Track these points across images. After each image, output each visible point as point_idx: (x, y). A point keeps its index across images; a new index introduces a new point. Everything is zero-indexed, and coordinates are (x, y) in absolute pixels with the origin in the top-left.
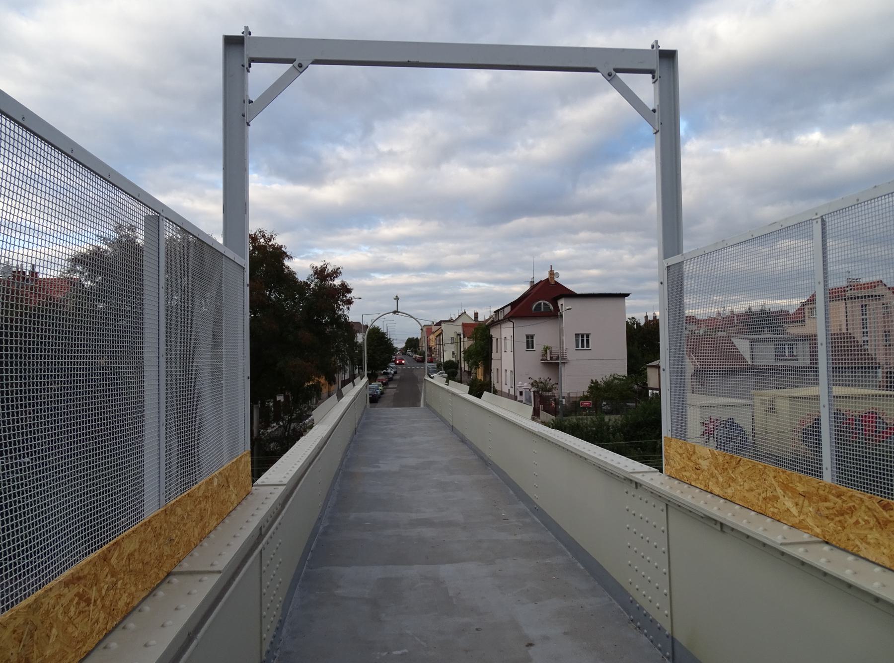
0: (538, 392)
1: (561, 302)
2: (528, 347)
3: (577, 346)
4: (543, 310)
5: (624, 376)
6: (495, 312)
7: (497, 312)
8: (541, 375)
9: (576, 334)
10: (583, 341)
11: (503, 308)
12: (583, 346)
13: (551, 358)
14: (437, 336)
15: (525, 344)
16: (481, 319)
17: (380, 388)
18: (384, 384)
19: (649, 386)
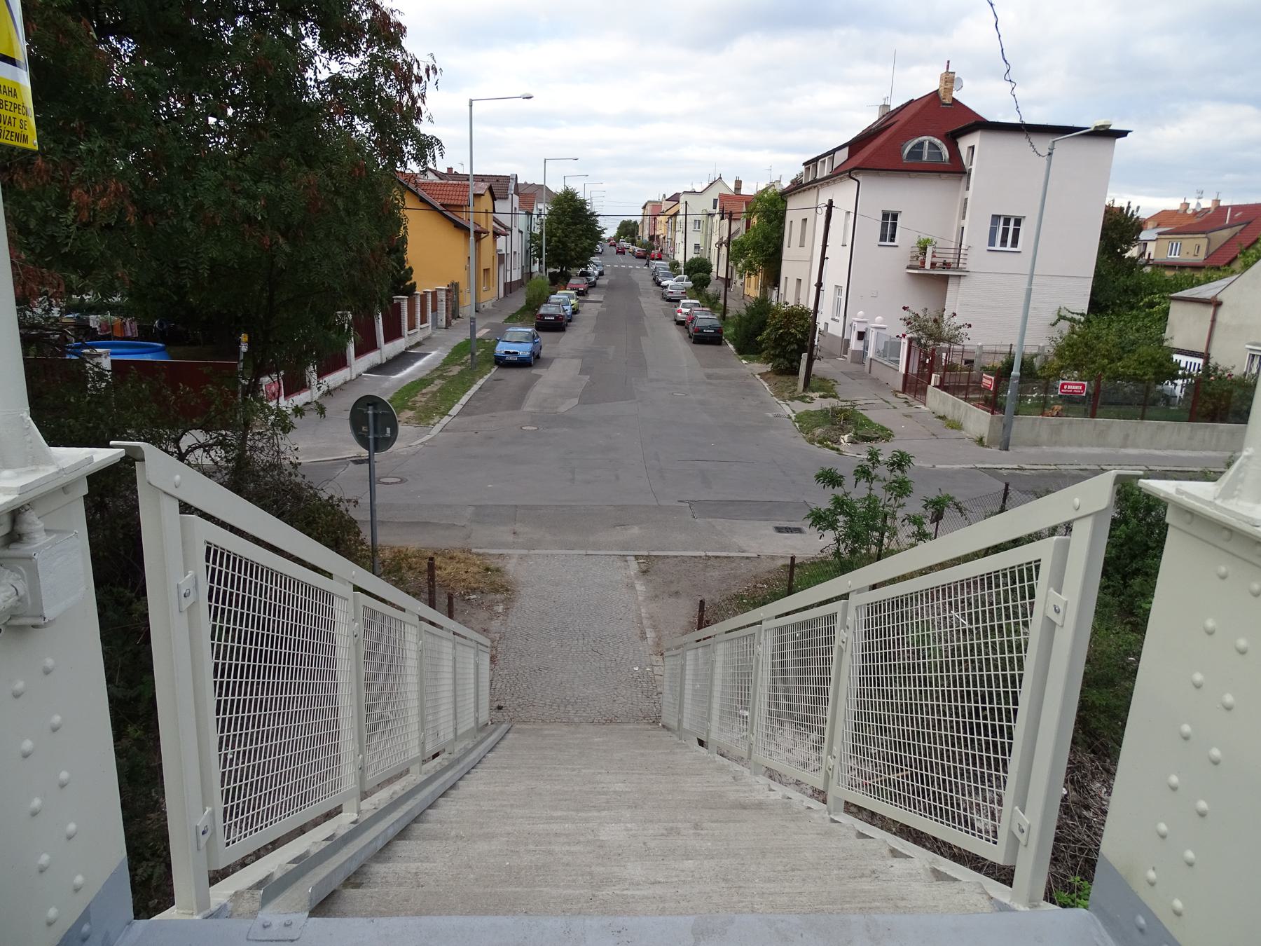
0: (919, 340)
1: (964, 144)
2: (883, 238)
3: (992, 243)
4: (925, 158)
5: (1082, 314)
6: (805, 164)
7: (811, 163)
8: (919, 303)
9: (993, 216)
10: (1005, 231)
12: (1004, 242)
13: (933, 265)
16: (745, 191)
17: (573, 301)
18: (580, 293)
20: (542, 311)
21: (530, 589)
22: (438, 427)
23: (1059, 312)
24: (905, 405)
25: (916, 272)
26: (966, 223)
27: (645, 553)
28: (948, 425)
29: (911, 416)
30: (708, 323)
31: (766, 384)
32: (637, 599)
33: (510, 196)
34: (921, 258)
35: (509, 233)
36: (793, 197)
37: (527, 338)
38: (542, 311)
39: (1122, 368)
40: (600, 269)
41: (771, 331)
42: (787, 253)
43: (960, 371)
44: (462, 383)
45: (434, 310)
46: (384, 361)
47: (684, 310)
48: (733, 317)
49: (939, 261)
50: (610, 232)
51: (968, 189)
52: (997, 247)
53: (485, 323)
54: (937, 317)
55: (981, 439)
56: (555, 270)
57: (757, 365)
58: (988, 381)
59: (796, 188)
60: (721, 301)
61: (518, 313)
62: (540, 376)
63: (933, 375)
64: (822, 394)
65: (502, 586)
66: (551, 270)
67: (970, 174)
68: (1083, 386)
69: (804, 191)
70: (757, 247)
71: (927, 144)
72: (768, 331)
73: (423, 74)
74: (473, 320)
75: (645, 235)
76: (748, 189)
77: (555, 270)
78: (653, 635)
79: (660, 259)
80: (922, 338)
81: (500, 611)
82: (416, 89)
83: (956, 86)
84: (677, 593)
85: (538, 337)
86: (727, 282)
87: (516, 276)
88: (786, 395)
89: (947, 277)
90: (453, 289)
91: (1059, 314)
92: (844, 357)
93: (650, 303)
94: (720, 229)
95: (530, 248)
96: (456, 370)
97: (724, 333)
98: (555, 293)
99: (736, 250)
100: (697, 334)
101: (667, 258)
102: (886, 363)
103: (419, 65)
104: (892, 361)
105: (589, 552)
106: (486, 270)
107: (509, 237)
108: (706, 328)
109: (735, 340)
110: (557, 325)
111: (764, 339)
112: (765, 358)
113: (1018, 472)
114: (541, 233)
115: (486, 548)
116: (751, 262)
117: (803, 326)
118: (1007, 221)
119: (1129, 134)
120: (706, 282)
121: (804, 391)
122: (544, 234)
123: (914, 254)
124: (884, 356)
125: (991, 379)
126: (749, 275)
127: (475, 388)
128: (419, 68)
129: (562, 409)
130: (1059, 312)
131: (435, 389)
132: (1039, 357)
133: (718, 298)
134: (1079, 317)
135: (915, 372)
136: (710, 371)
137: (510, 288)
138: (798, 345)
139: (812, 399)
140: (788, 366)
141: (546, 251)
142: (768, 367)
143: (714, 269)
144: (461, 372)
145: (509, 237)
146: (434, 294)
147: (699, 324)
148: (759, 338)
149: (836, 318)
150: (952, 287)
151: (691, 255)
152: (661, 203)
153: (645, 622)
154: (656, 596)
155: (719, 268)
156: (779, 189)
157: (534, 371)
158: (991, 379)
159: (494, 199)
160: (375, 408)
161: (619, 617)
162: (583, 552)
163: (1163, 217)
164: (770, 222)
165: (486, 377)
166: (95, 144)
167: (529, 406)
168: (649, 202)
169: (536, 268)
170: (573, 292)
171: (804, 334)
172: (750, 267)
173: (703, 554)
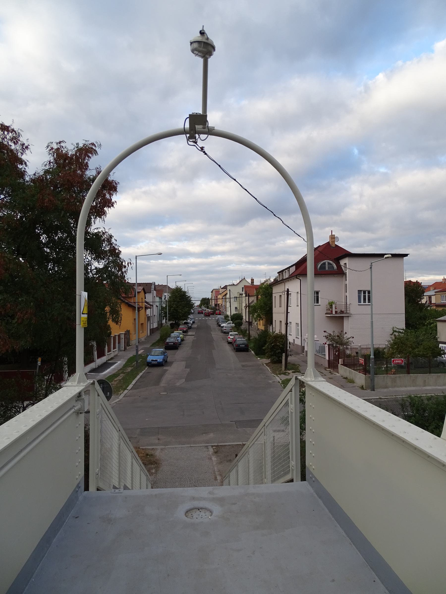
0: (332, 345)
1: (342, 262)
3: (360, 301)
4: (327, 269)
5: (403, 329)
6: (278, 273)
7: (281, 272)
8: (332, 329)
9: (358, 290)
10: (365, 297)
11: (289, 268)
12: (365, 301)
14: (224, 296)
16: (256, 283)
17: (181, 336)
18: (184, 332)
19: (439, 340)
20: (168, 341)
21: (166, 462)
22: (122, 395)
23: (393, 329)
24: (330, 374)
25: (329, 315)
26: (348, 294)
27: (216, 444)
28: (348, 381)
29: (332, 378)
30: (241, 342)
31: (268, 368)
32: (213, 463)
33: (152, 291)
34: (331, 310)
35: (152, 307)
36: (275, 286)
37: (161, 353)
38: (168, 341)
39: (418, 352)
40: (193, 320)
41: (269, 344)
42: (274, 310)
43: (354, 357)
44: (133, 375)
45: (119, 343)
46: (97, 367)
47: (231, 337)
48: (253, 339)
49: (339, 311)
50: (198, 303)
51: (346, 280)
52: (362, 303)
53: (142, 348)
54: (339, 335)
55: (362, 386)
56: (172, 322)
57: (264, 360)
58: (362, 361)
59: (276, 283)
60: (248, 332)
61: (156, 342)
62: (167, 370)
63: (340, 360)
64: (293, 371)
65: (154, 462)
66: (171, 322)
67: (346, 274)
68: (402, 360)
69: (279, 284)
70: (261, 308)
71: (327, 263)
72: (267, 344)
73: (126, 265)
74: (137, 347)
75: (213, 303)
76: (257, 282)
77: (172, 322)
78: (220, 478)
79: (220, 314)
80: (334, 344)
81: (154, 472)
82: (124, 270)
83: (336, 240)
84: (230, 460)
85: (166, 352)
86: (250, 323)
87: (155, 325)
88: (278, 372)
89: (343, 316)
90: (128, 333)
91: (393, 330)
92: (303, 354)
93: (216, 335)
94: (245, 301)
95: (161, 313)
96: (129, 369)
97: (249, 346)
98: (173, 332)
99: (252, 309)
100: (237, 347)
101: (223, 314)
102: (320, 356)
103: (125, 262)
104: (323, 354)
105: (191, 445)
106: (142, 324)
107: (152, 309)
108: (241, 344)
109: (254, 349)
110: (175, 347)
111: (266, 348)
112: (267, 357)
113: (379, 400)
114: (166, 306)
115: (146, 446)
116: (259, 314)
117: (282, 342)
118: (365, 292)
120: (241, 324)
121: (285, 370)
122: (167, 307)
123: (328, 308)
124: (319, 353)
125: (362, 360)
126: (259, 320)
127: (138, 377)
128: (125, 263)
129: (178, 384)
130: (393, 329)
131: (120, 378)
132: (386, 349)
133: (246, 331)
134: (402, 330)
135: (333, 359)
136: (244, 364)
137: (153, 331)
138: (281, 350)
139: (289, 373)
140: (277, 359)
141: (169, 314)
142: (268, 361)
143: (244, 318)
144: (132, 370)
145: (152, 309)
146: (119, 336)
147: (238, 343)
148: (264, 348)
149: (298, 337)
150: (345, 322)
151: (234, 312)
152: (219, 289)
153: (216, 473)
154: (221, 462)
155: (245, 317)
156: (269, 283)
157: (165, 368)
158: (362, 360)
159: (145, 293)
160: (103, 385)
161: (205, 471)
162: (189, 445)
163: (436, 285)
164: (266, 297)
165: (143, 372)
166: (24, 298)
167: (163, 384)
168: (214, 289)
169: (164, 321)
170: (181, 332)
171: (283, 345)
172: (259, 316)
173: (241, 443)
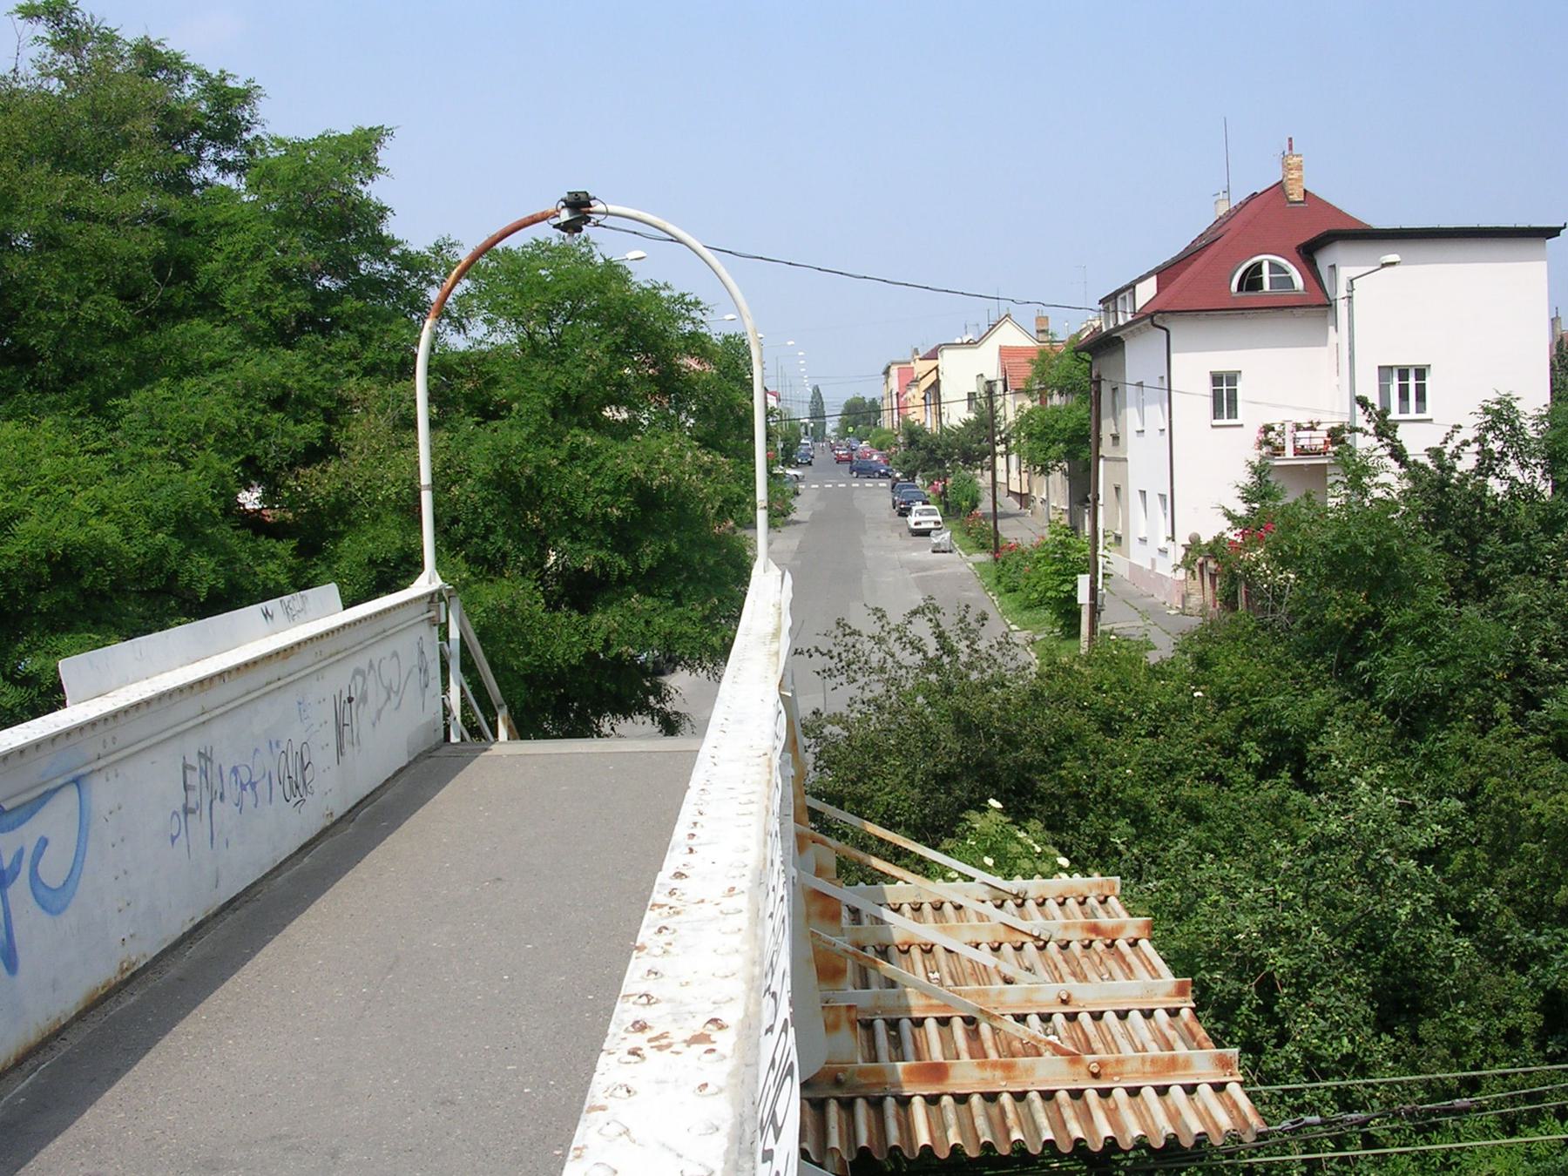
2: (1217, 413)
4: (1267, 286)
14: (926, 391)
15: (1208, 404)
119: (1562, 232)
